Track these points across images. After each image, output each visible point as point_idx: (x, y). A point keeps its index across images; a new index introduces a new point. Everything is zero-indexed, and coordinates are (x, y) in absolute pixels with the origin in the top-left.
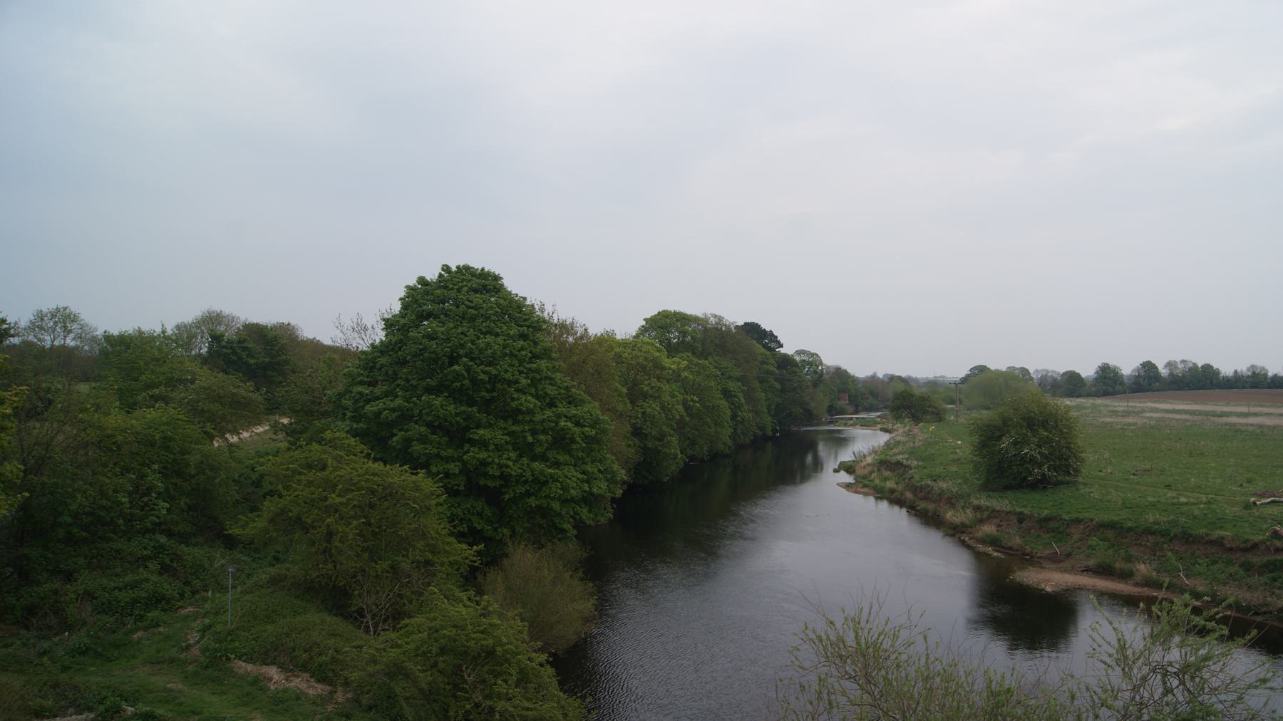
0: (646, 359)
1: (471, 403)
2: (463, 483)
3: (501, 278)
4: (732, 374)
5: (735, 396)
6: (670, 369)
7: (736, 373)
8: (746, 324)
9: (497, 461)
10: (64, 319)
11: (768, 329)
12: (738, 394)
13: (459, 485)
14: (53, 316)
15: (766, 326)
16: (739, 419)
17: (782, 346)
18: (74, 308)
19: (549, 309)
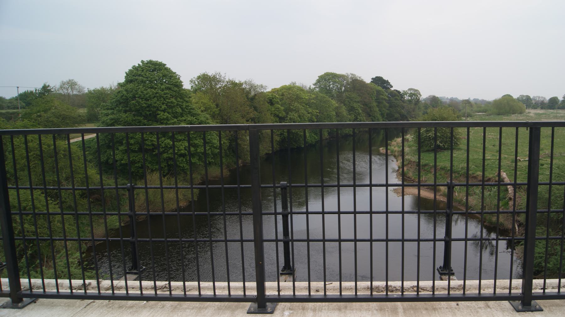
0: (293, 95)
1: (141, 115)
2: (137, 148)
3: (166, 65)
4: (356, 100)
5: (357, 110)
6: (305, 98)
7: (359, 99)
8: (377, 77)
9: (150, 139)
10: (72, 84)
11: (386, 80)
12: (358, 109)
13: (135, 148)
14: (68, 83)
15: (385, 78)
16: (358, 119)
17: (392, 87)
18: (76, 80)
19: (223, 75)
